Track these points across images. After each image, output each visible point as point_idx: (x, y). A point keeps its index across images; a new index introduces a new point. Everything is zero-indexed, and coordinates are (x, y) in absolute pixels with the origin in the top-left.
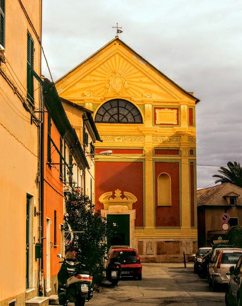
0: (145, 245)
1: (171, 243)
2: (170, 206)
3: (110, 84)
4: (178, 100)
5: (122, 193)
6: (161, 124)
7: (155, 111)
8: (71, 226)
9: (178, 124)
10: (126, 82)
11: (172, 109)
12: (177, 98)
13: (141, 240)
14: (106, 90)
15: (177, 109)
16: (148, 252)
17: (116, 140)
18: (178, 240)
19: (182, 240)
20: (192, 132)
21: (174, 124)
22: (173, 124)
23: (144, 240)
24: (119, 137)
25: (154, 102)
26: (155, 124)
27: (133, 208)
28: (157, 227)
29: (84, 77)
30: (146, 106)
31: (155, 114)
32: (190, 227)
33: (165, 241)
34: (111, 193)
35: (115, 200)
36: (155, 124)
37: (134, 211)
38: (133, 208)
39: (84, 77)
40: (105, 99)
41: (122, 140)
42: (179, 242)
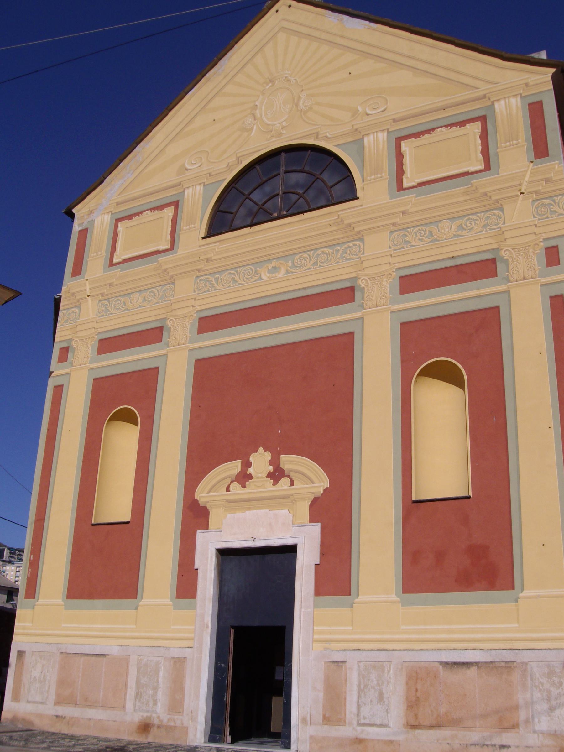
0: (353, 678)
1: (474, 670)
2: (468, 498)
3: (258, 115)
4: (484, 88)
5: (275, 462)
6: (421, 184)
7: (398, 147)
8: (11, 601)
9: (488, 167)
10: (303, 95)
11: (462, 124)
12: (562, 206)
13: (338, 657)
14: (246, 134)
15: (483, 119)
16: (365, 711)
17: (265, 276)
18: (508, 656)
19: (525, 657)
20: (547, 180)
21: (472, 169)
22: (467, 174)
23: (352, 659)
24: (274, 263)
25: (394, 121)
26: (400, 187)
27: (312, 520)
28: (18, 588)
29: (186, 125)
30: (368, 141)
31: (400, 156)
32: (60, 601)
33: (446, 664)
34: (235, 467)
35: (252, 488)
36: (400, 187)
37: (317, 528)
38: (312, 520)
39: (186, 125)
40: (239, 161)
41: (283, 271)
42: (509, 666)
